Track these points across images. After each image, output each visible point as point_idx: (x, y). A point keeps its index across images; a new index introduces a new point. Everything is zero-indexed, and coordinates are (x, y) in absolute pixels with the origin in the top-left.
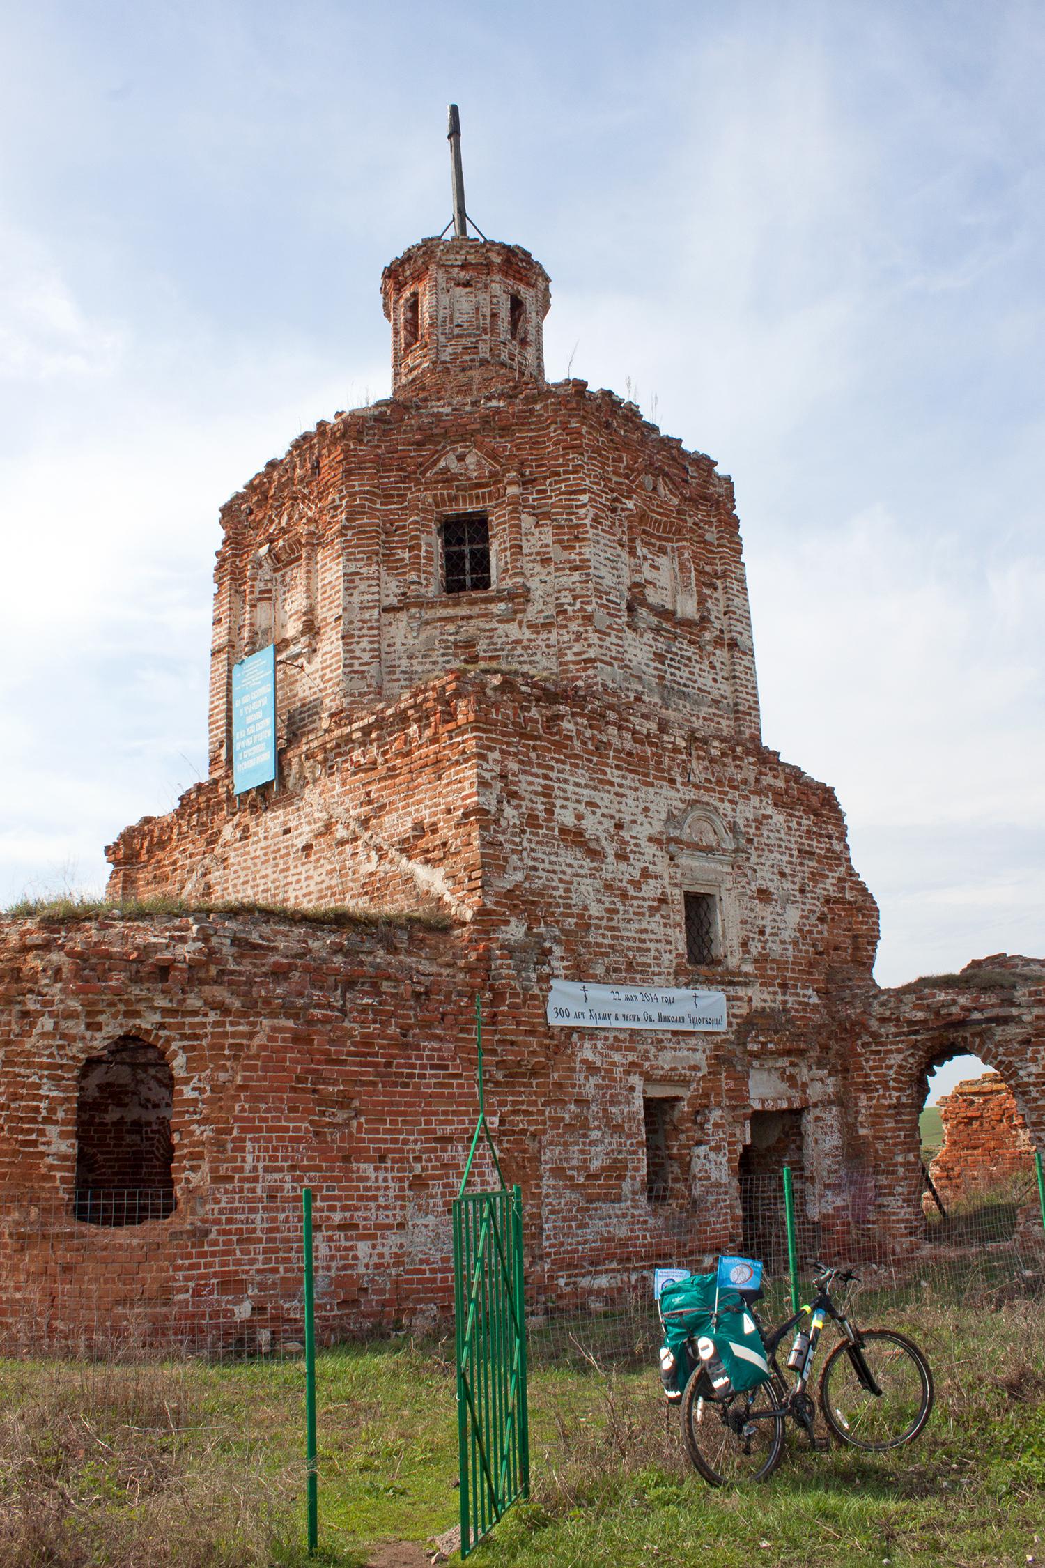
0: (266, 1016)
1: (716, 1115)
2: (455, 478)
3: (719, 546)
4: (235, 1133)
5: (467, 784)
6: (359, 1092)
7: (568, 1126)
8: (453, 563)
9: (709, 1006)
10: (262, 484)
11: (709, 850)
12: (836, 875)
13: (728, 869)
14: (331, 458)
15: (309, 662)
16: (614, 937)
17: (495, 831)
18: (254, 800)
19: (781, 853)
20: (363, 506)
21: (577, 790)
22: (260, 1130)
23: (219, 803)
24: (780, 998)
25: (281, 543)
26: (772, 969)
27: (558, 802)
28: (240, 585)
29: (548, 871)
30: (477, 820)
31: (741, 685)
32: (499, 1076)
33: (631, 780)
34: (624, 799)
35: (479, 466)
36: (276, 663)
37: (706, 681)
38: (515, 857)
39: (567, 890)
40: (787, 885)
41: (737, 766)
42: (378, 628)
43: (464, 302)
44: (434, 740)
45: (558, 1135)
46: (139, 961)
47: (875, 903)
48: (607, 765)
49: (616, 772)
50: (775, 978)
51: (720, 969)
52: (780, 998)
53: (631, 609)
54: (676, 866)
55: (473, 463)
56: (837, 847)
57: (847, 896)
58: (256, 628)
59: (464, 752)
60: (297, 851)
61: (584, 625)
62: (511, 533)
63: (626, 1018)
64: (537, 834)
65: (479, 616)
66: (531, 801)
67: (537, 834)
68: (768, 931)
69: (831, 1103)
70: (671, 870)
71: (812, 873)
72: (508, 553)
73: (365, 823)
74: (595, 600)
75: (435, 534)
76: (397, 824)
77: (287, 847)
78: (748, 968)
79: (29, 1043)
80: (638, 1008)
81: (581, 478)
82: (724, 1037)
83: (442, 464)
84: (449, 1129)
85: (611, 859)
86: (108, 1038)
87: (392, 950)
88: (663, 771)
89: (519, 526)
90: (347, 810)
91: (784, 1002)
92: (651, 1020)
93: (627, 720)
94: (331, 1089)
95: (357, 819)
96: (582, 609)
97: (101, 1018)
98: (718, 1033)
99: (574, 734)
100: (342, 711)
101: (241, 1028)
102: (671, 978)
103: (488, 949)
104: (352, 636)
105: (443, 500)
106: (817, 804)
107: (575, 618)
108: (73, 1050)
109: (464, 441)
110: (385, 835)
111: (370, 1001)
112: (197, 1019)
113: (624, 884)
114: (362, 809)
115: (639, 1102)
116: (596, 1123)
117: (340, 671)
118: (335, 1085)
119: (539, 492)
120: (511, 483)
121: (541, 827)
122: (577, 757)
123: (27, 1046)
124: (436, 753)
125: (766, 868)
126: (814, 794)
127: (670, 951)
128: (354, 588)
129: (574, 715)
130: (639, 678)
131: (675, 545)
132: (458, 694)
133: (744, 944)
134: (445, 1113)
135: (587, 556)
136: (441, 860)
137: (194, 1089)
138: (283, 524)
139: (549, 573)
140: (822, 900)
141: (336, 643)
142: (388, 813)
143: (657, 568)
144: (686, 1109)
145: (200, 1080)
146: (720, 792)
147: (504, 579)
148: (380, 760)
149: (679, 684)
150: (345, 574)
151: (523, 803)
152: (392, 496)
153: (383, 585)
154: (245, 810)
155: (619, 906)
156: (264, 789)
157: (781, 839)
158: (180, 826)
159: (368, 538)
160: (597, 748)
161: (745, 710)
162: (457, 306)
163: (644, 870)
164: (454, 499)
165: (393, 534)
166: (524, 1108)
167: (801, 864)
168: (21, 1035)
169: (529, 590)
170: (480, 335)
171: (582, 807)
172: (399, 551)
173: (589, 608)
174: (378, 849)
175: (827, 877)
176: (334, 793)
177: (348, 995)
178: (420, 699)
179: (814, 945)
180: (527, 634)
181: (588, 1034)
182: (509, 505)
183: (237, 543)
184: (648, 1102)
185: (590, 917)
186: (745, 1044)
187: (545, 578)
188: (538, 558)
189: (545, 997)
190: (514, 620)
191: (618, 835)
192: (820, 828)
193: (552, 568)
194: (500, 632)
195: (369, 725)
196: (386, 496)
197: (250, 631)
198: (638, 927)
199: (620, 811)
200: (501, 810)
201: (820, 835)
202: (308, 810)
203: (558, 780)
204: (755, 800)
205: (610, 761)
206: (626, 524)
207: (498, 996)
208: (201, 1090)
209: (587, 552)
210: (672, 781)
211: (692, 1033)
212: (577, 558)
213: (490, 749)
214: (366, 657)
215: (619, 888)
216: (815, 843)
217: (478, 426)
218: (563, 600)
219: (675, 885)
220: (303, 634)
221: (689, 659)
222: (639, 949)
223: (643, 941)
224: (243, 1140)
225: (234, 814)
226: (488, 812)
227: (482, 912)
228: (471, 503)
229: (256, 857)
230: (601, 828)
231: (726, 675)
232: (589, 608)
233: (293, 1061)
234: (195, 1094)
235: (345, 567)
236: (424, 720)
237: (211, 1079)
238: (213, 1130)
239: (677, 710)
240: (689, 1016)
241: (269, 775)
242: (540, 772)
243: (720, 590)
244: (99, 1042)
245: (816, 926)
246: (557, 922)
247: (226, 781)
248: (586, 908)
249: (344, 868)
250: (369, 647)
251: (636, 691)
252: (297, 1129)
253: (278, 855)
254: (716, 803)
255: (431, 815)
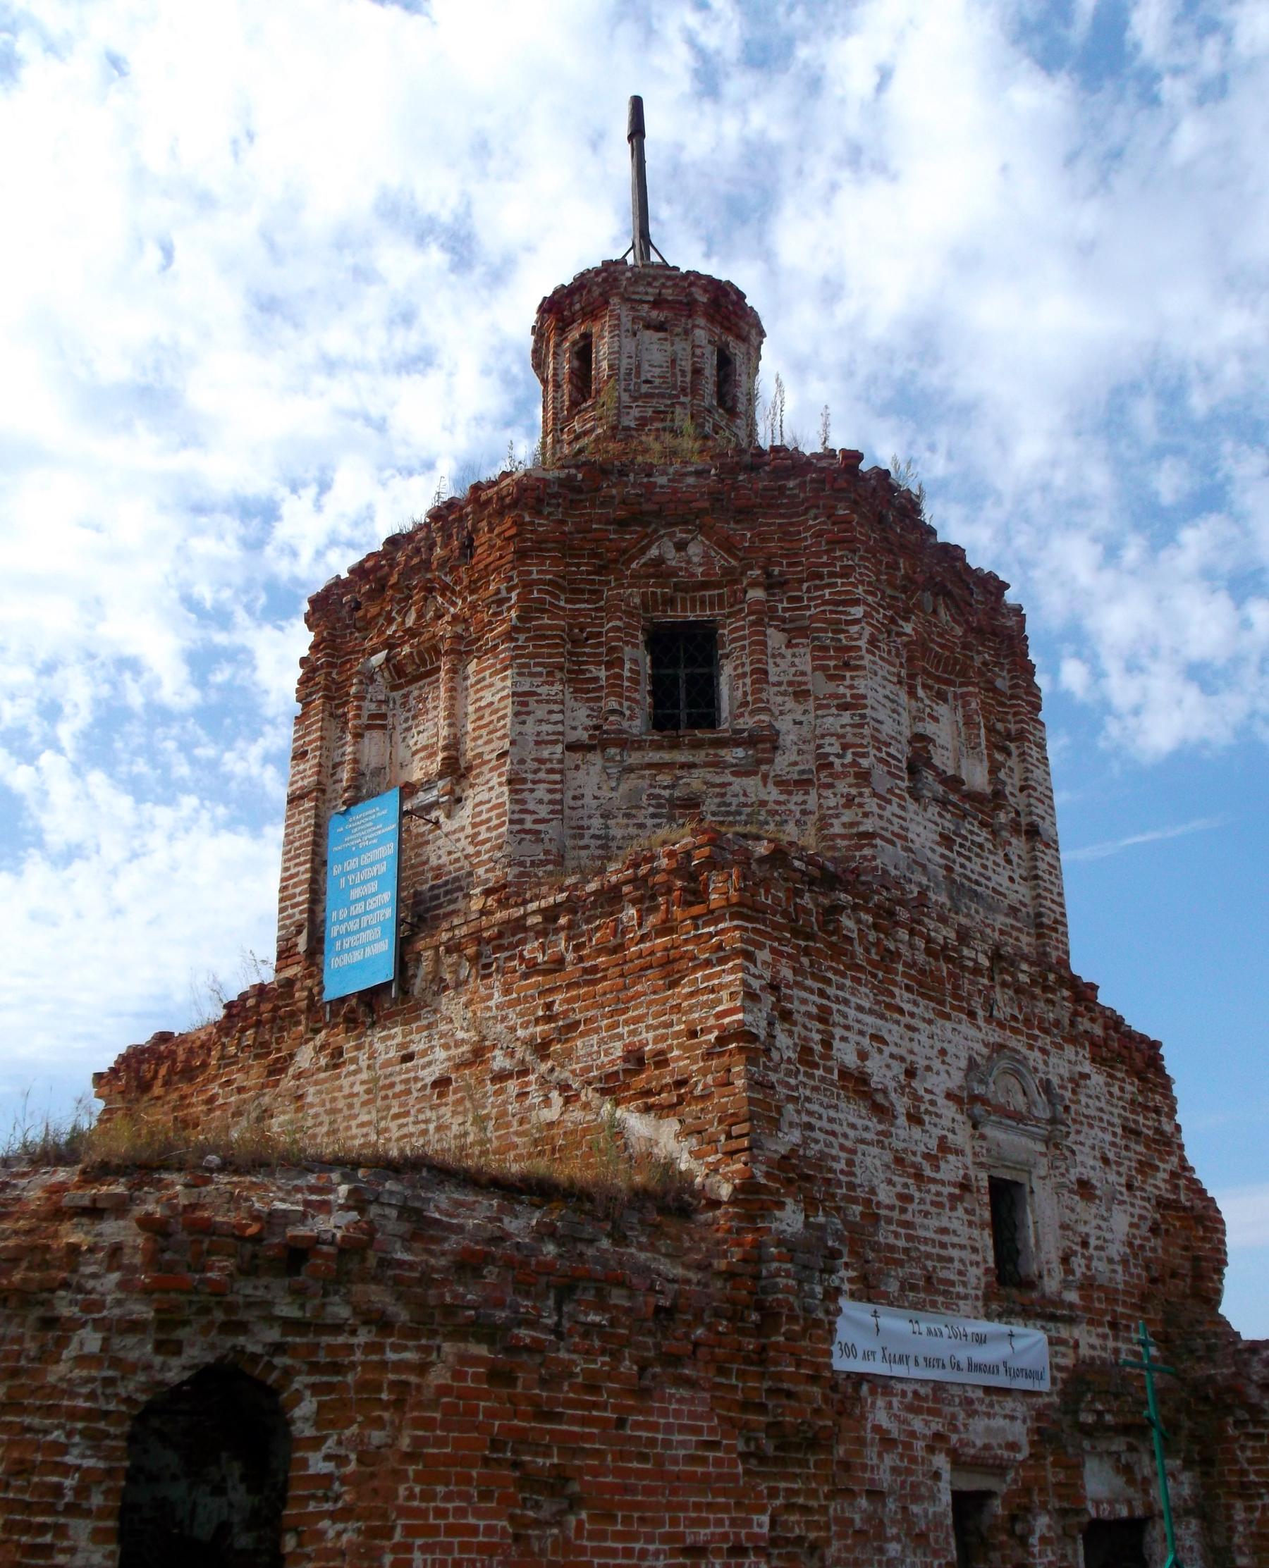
0: (448, 1337)
1: (1042, 1523)
2: (673, 572)
3: (1012, 697)
4: (398, 1536)
5: (724, 994)
6: (579, 1469)
7: (859, 1533)
8: (662, 692)
9: (1025, 1347)
10: (377, 567)
11: (1018, 1117)
12: (1168, 1167)
13: (1040, 1147)
14: (490, 539)
15: (448, 816)
16: (909, 1238)
17: (766, 1067)
18: (352, 1011)
19: (1103, 1130)
20: (542, 601)
21: (861, 1016)
22: (434, 1530)
23: (292, 1014)
24: (1111, 1344)
25: (406, 649)
26: (1099, 1299)
27: (838, 1032)
28: (338, 707)
29: (827, 1132)
30: (740, 1049)
31: (1046, 889)
32: (769, 1448)
33: (924, 1008)
34: (916, 1035)
35: (707, 560)
36: (403, 814)
37: (1000, 879)
38: (790, 1107)
39: (850, 1163)
40: (1112, 1177)
41: (1049, 1001)
42: (561, 772)
43: (655, 352)
44: (666, 928)
45: (848, 1549)
46: (257, 1239)
47: (1218, 1212)
48: (895, 983)
49: (906, 995)
50: (1104, 1312)
51: (1035, 1295)
52: (1111, 1344)
53: (913, 770)
54: (983, 1137)
55: (697, 556)
56: (1168, 1128)
57: (1183, 1198)
58: (362, 767)
59: (719, 947)
60: (424, 1087)
61: (857, 785)
62: (752, 653)
63: (930, 1363)
64: (812, 1076)
65: (706, 765)
66: (805, 1027)
67: (812, 1076)
68: (1093, 1242)
69: (1188, 1512)
70: (977, 1143)
71: (1140, 1162)
72: (748, 680)
73: (541, 1049)
74: (873, 752)
75: (642, 647)
76: (599, 1050)
77: (406, 1081)
78: (1072, 1296)
79: (56, 1373)
80: (943, 1348)
81: (851, 584)
82: (1047, 1400)
83: (654, 552)
84: (704, 1533)
85: (902, 1120)
86: (190, 1368)
87: (620, 1238)
88: (960, 998)
89: (764, 644)
90: (513, 1029)
91: (1116, 1351)
92: (959, 1369)
93: (920, 922)
94: (540, 1461)
95: (529, 1042)
96: (854, 764)
97: (182, 1333)
98: (1037, 1394)
99: (855, 935)
100: (504, 886)
101: (408, 1355)
102: (980, 1304)
103: (758, 1245)
104: (524, 781)
105: (656, 601)
106: (1137, 1061)
107: (845, 775)
108: (129, 1387)
109: (686, 523)
110: (577, 1067)
111: (597, 1319)
112: (341, 1339)
113: (919, 1159)
114: (538, 1029)
115: (946, 1498)
116: (894, 1531)
117: (504, 829)
118: (547, 1455)
119: (792, 599)
120: (754, 584)
121: (816, 1066)
122: (859, 968)
123: (51, 1379)
124: (666, 949)
125: (1086, 1149)
126: (1138, 1050)
127: (977, 1264)
128: (528, 713)
129: (855, 907)
130: (924, 867)
131: (959, 691)
132: (711, 863)
133: (1065, 1260)
134: (698, 1507)
135: (862, 691)
136: (672, 1106)
137: (328, 1458)
138: (410, 621)
139: (805, 712)
140: (1153, 1202)
141: (498, 790)
142: (582, 1035)
143: (936, 720)
144: (1000, 1511)
145: (339, 1443)
146: (1029, 1036)
147: (742, 715)
148: (570, 957)
149: (969, 879)
150: (514, 694)
151: (795, 1029)
152: (582, 591)
153: (568, 713)
154: (336, 1025)
155: (913, 1190)
156: (371, 998)
157: (1101, 1110)
158: (224, 1046)
159: (548, 646)
160: (882, 959)
161: (1047, 925)
162: (646, 356)
163: (942, 1139)
164: (670, 602)
165: (584, 642)
166: (801, 1501)
167: (1127, 1148)
168: (38, 1359)
169: (778, 733)
170: (677, 396)
171: (866, 1042)
172: (592, 667)
173: (865, 763)
174: (564, 1087)
175: (1157, 1168)
176: (492, 1003)
177: (565, 1309)
178: (644, 869)
179: (1147, 1268)
180: (773, 794)
181: (881, 1384)
182: (750, 614)
183: (334, 648)
184: (958, 1496)
185: (878, 1203)
186: (1076, 1413)
187: (800, 718)
188: (790, 689)
189: (832, 1323)
190: (756, 773)
191: (909, 1086)
192: (1146, 1097)
193: (811, 704)
194: (736, 788)
195: (557, 905)
196: (573, 591)
197: (353, 770)
198: (937, 1224)
199: (911, 1052)
200: (772, 1036)
201: (1146, 1108)
202: (444, 1027)
203: (837, 1000)
204: (1069, 1050)
205: (899, 978)
206: (904, 653)
207: (770, 1317)
208: (341, 1460)
209: (862, 686)
210: (972, 1014)
211: (1006, 1392)
212: (848, 692)
213: (761, 946)
214: (543, 811)
215: (913, 1165)
216: (1141, 1119)
217: (707, 505)
218: (827, 749)
219: (981, 1165)
220: (441, 775)
221: (981, 846)
222: (941, 1258)
223: (943, 1246)
224: (409, 1548)
225: (317, 1031)
226: (755, 1038)
227: (747, 1190)
228: (693, 610)
229: (352, 1095)
230: (889, 1074)
231: (1025, 874)
232: (865, 763)
233: (491, 1414)
234: (328, 1467)
235: (514, 684)
236: (646, 902)
237: (359, 1443)
238: (358, 1531)
239: (968, 915)
240: (1005, 1363)
241: (384, 972)
242: (816, 985)
243: (1015, 757)
244: (174, 1372)
245: (1147, 1239)
246: (838, 1209)
247: (309, 982)
248: (873, 1191)
249: (503, 1114)
250: (547, 797)
251: (920, 884)
252: (490, 1530)
253: (390, 1093)
254: (1024, 1050)
255: (656, 1040)
